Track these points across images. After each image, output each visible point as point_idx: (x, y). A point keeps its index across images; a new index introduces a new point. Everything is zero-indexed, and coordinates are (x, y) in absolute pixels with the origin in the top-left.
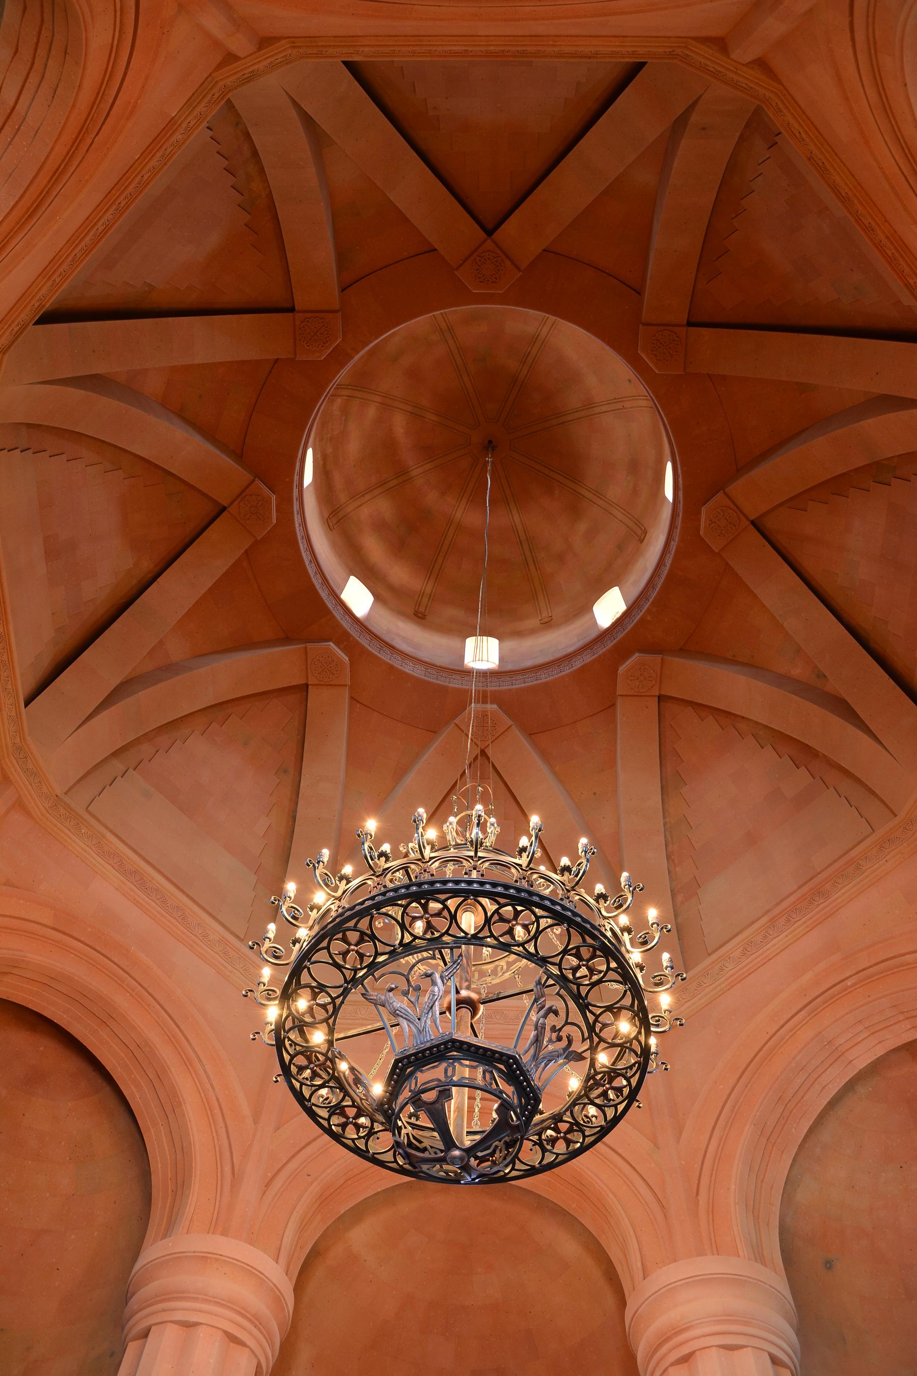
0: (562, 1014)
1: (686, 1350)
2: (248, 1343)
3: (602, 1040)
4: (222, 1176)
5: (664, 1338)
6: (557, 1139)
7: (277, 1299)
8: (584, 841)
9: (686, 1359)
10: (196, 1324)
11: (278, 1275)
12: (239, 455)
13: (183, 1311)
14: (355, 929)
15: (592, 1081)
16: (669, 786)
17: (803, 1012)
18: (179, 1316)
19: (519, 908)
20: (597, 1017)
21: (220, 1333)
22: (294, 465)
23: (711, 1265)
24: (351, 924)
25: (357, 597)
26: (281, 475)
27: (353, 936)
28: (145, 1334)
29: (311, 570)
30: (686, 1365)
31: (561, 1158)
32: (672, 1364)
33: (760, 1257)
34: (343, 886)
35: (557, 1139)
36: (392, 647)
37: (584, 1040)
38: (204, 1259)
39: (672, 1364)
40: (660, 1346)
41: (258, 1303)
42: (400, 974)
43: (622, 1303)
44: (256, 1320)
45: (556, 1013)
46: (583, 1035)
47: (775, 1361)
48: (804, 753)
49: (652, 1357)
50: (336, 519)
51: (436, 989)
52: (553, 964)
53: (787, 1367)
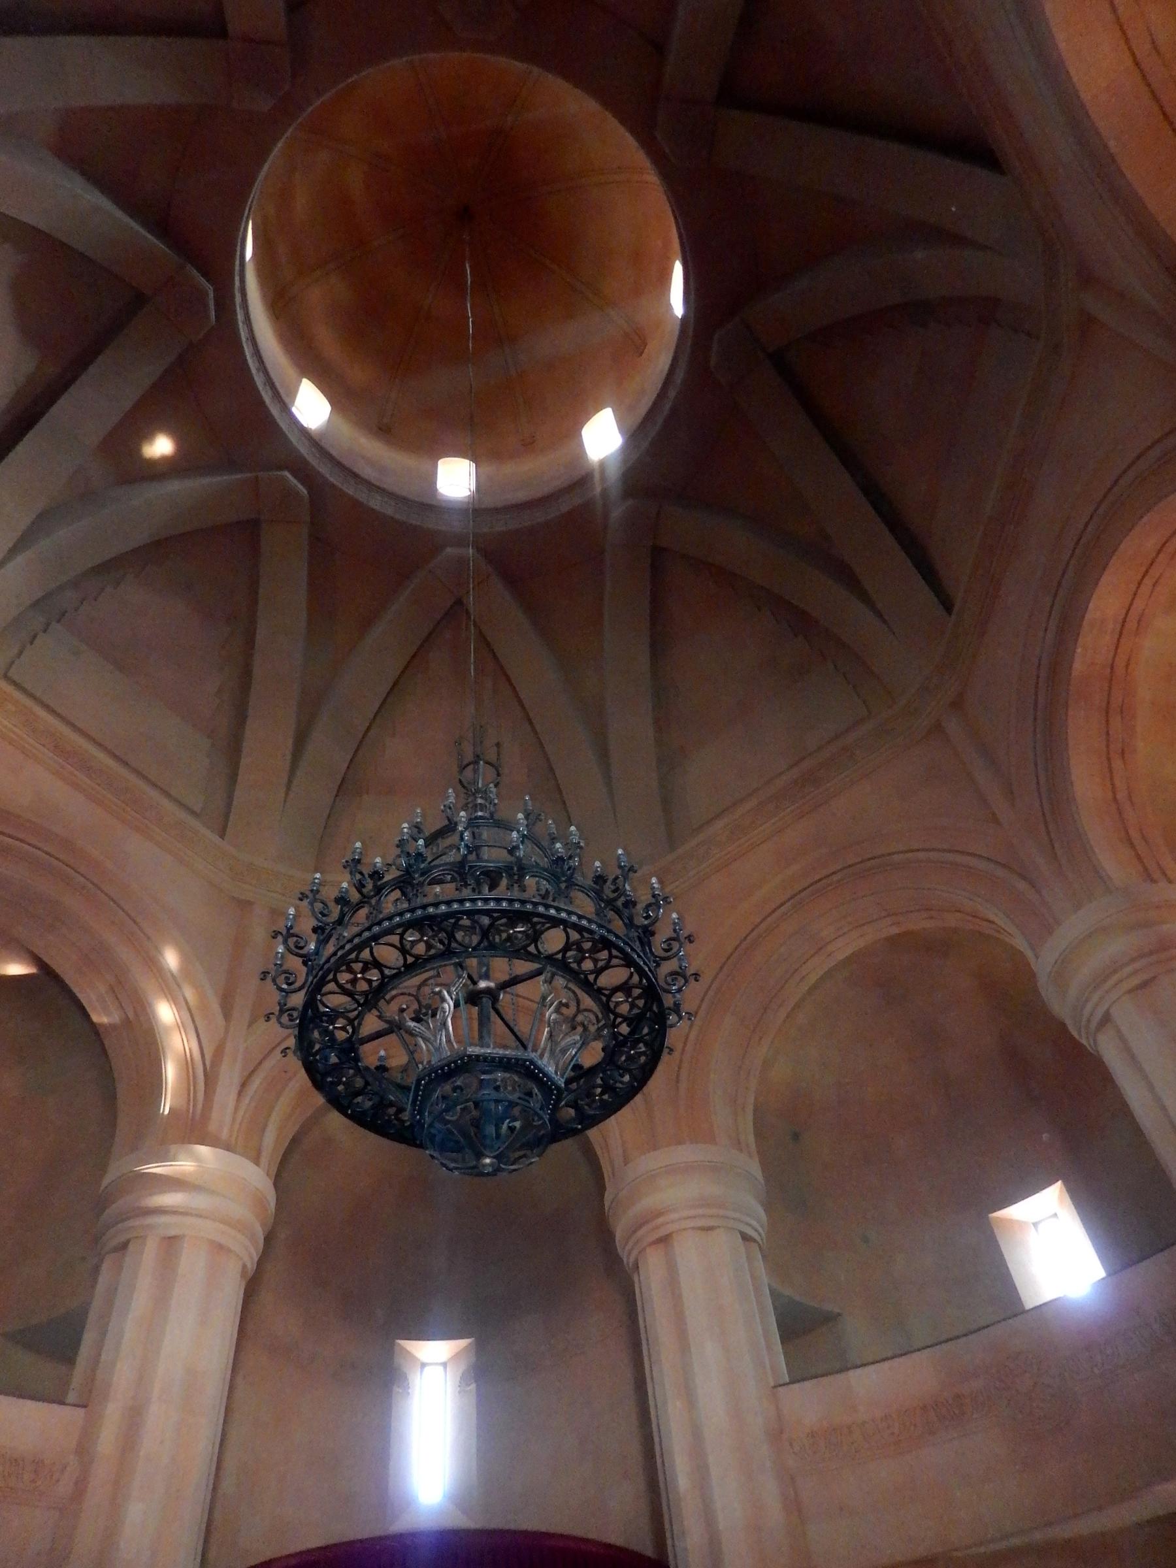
0: (573, 1004)
1: (662, 1232)
4: (195, 1092)
12: (163, 226)
14: (357, 960)
16: (658, 648)
17: (789, 904)
22: (233, 244)
23: (685, 1153)
24: (353, 956)
25: (311, 407)
26: (219, 265)
27: (358, 966)
28: (124, 1246)
29: (259, 380)
33: (738, 1144)
36: (356, 476)
40: (634, 1232)
42: (409, 995)
43: (601, 1188)
45: (567, 1005)
46: (597, 1017)
47: (745, 1238)
48: (801, 622)
49: (629, 1238)
50: (281, 304)
51: (446, 1006)
53: (755, 1241)
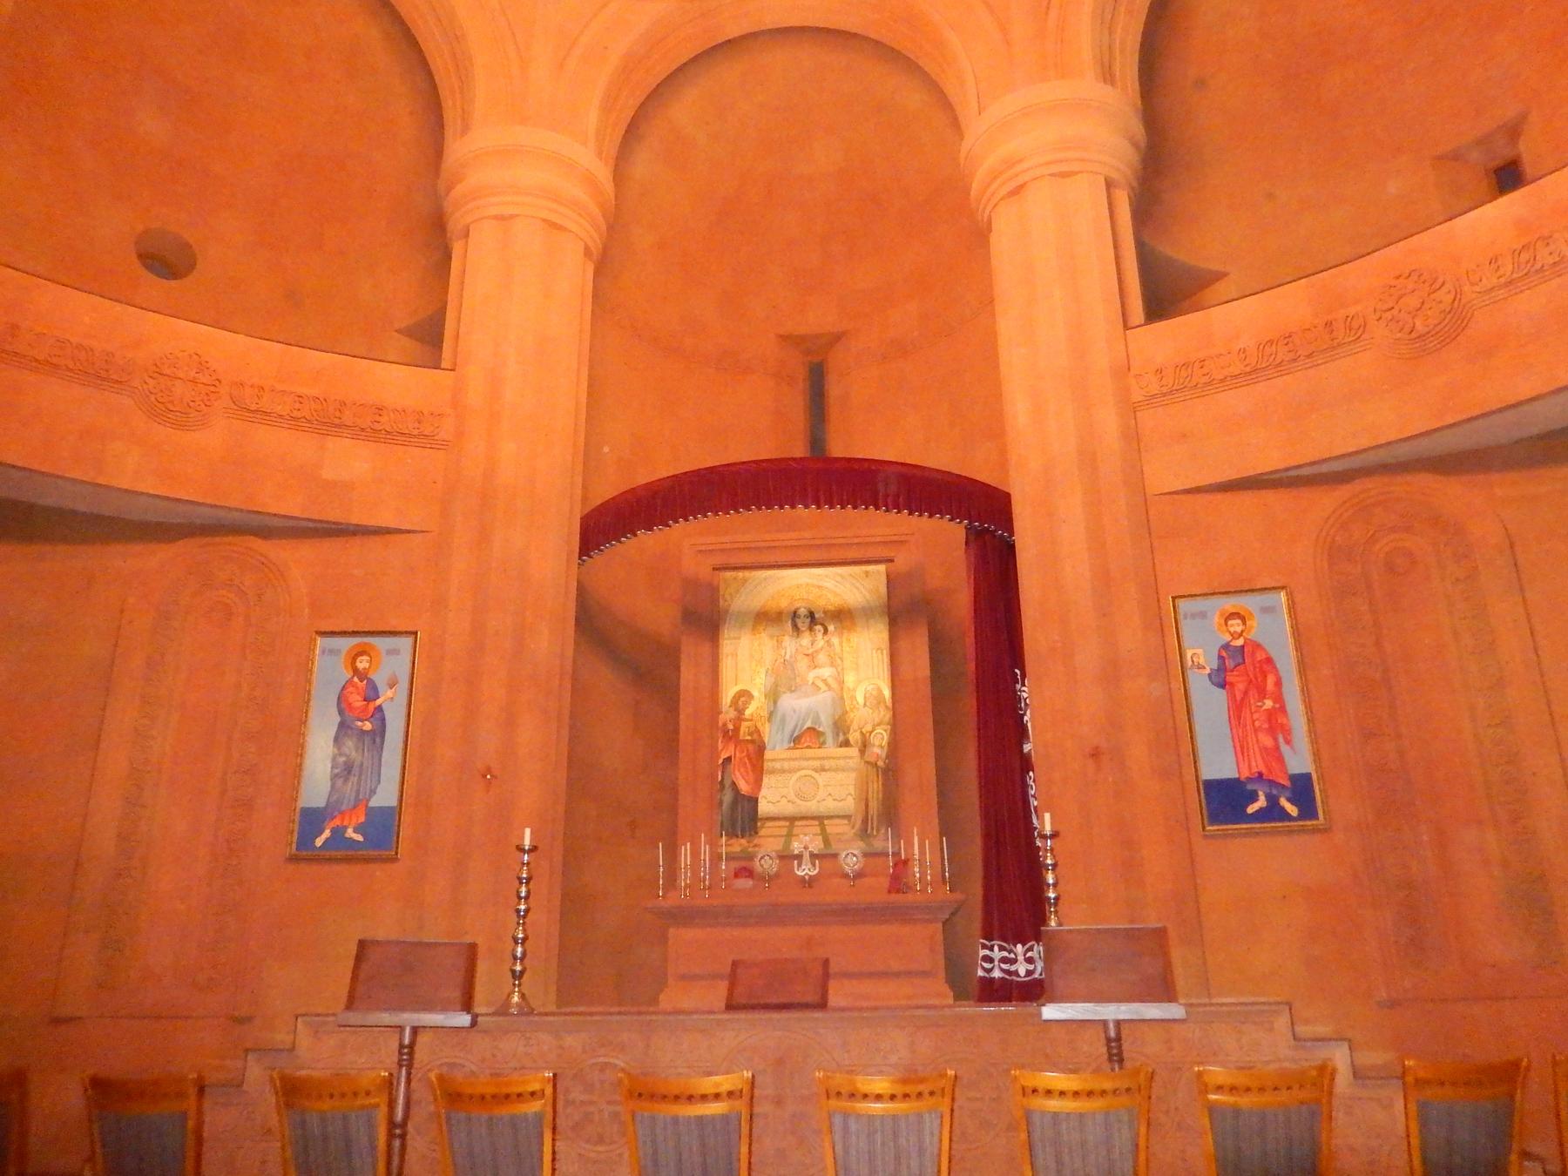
7: (590, 181)
10: (512, 217)
18: (493, 211)
28: (466, 234)
33: (1108, 76)
40: (989, 185)
41: (578, 192)
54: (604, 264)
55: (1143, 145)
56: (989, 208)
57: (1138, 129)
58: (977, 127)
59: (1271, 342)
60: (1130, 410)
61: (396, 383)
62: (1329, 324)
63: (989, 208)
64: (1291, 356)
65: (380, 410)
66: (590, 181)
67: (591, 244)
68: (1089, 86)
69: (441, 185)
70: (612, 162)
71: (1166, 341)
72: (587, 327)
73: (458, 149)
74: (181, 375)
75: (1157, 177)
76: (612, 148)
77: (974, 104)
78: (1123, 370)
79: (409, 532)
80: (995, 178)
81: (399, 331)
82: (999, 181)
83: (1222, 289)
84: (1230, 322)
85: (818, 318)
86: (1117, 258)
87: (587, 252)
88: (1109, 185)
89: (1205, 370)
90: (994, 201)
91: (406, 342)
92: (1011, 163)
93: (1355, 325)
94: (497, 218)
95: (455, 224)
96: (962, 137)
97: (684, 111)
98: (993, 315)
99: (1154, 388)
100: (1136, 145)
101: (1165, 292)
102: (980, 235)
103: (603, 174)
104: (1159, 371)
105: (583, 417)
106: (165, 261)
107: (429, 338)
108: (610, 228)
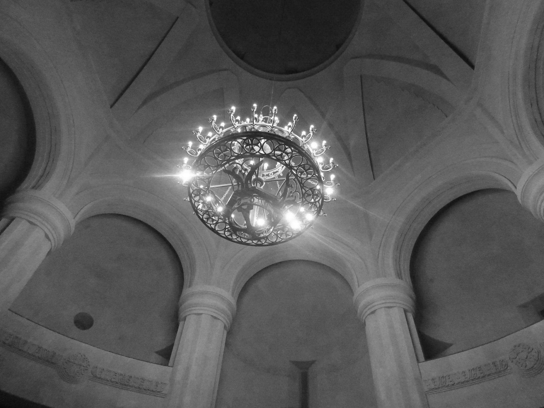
1: (373, 310)
2: (221, 318)
3: (306, 200)
5: (366, 306)
6: (283, 234)
7: (229, 304)
8: (295, 115)
9: (373, 313)
10: (202, 314)
11: (230, 297)
13: (197, 310)
15: (210, 206)
19: (287, 147)
20: (306, 191)
21: (210, 316)
23: (380, 281)
28: (185, 319)
30: (373, 315)
31: (283, 240)
32: (26, 220)
34: (208, 140)
35: (283, 234)
37: (300, 198)
38: (202, 293)
39: (368, 315)
41: (224, 307)
44: (223, 311)
52: (294, 170)
54: (230, 332)
55: (414, 298)
56: (364, 318)
57: (413, 295)
58: (358, 290)
59: (473, 369)
60: (424, 395)
61: (152, 371)
62: (494, 363)
63: (364, 318)
64: (482, 375)
65: (143, 380)
66: (229, 304)
67: (226, 324)
68: (392, 279)
69: (181, 301)
70: (236, 298)
71: (432, 368)
72: (222, 354)
73: (186, 291)
74: (76, 362)
75: (421, 310)
76: (237, 295)
77: (356, 283)
78: (419, 380)
79: (117, 100)
80: (366, 308)
81: (157, 352)
82: (367, 308)
83: (452, 349)
84: (458, 362)
85: (305, 356)
86: (410, 330)
87: (225, 327)
88: (405, 311)
89: (450, 380)
90: (366, 315)
91: (157, 356)
92: (369, 303)
93: (504, 363)
94: (196, 314)
95: (182, 315)
96: (353, 295)
97: (261, 283)
98: (369, 358)
99: (433, 386)
100: (411, 298)
101: (431, 349)
102: (363, 326)
103: (233, 302)
104: (433, 379)
105: (217, 384)
106: (84, 323)
107: (166, 355)
108: (233, 320)
